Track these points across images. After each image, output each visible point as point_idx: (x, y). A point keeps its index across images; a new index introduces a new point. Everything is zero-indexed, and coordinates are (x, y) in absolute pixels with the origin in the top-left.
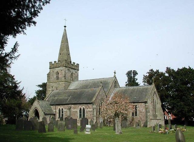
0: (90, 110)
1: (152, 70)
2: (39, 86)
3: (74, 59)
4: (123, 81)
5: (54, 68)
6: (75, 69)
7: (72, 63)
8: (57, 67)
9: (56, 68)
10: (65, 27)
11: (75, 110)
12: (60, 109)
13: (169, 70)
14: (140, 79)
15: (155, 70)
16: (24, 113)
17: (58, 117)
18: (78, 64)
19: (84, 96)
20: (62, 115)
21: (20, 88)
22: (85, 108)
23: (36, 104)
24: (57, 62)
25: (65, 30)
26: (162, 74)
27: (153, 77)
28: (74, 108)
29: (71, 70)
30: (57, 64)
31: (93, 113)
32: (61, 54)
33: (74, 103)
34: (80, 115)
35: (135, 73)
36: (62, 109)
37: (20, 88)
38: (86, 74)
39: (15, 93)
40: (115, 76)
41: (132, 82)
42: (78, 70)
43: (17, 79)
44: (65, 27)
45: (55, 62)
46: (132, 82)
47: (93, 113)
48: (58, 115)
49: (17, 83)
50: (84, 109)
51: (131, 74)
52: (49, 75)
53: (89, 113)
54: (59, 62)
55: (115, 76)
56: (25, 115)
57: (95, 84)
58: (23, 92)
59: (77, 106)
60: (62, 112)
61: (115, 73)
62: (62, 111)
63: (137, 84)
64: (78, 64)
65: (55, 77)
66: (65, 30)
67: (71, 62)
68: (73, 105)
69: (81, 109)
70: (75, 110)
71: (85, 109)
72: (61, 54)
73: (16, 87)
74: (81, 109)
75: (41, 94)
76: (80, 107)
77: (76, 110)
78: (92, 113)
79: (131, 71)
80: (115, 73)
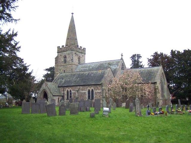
0: (99, 91)
1: (156, 53)
2: (47, 70)
3: (81, 43)
4: (128, 64)
5: (61, 52)
6: (82, 53)
7: (79, 47)
8: (65, 51)
9: (64, 52)
10: (72, 14)
11: (83, 92)
12: (68, 91)
13: (173, 52)
14: (145, 62)
15: (159, 53)
16: (33, 96)
17: (66, 98)
18: (84, 49)
19: (94, 78)
20: (71, 97)
21: (152, 58)
22: (93, 89)
23: (44, 86)
24: (65, 47)
25: (72, 16)
26: (166, 57)
27: (157, 59)
28: (83, 90)
29: (78, 53)
30: (64, 48)
31: (103, 94)
32: (68, 39)
33: (82, 84)
34: (89, 97)
35: (139, 56)
36: (71, 91)
37: (152, 58)
38: (92, 57)
39: (23, 75)
40: (122, 59)
41: (136, 64)
42: (85, 54)
43: (26, 62)
44: (72, 14)
45: (63, 46)
46: (136, 64)
47: (103, 94)
48: (66, 97)
49: (26, 65)
50: (92, 90)
51: (135, 58)
52: (57, 59)
53: (98, 94)
54: (67, 46)
55: (122, 59)
56: (34, 98)
57: (102, 66)
58: (32, 75)
59: (85, 87)
60: (71, 94)
61: (122, 55)
62: (70, 93)
63: (141, 66)
64: (84, 49)
65: (63, 60)
66: (72, 16)
67: (78, 46)
68: (81, 87)
69: (89, 90)
70: (83, 92)
71: (94, 91)
72: (68, 39)
73: (26, 69)
74: (89, 90)
75: (51, 75)
76: (67, 89)
77: (85, 91)
78: (102, 94)
79: (136, 54)
80: (122, 55)
